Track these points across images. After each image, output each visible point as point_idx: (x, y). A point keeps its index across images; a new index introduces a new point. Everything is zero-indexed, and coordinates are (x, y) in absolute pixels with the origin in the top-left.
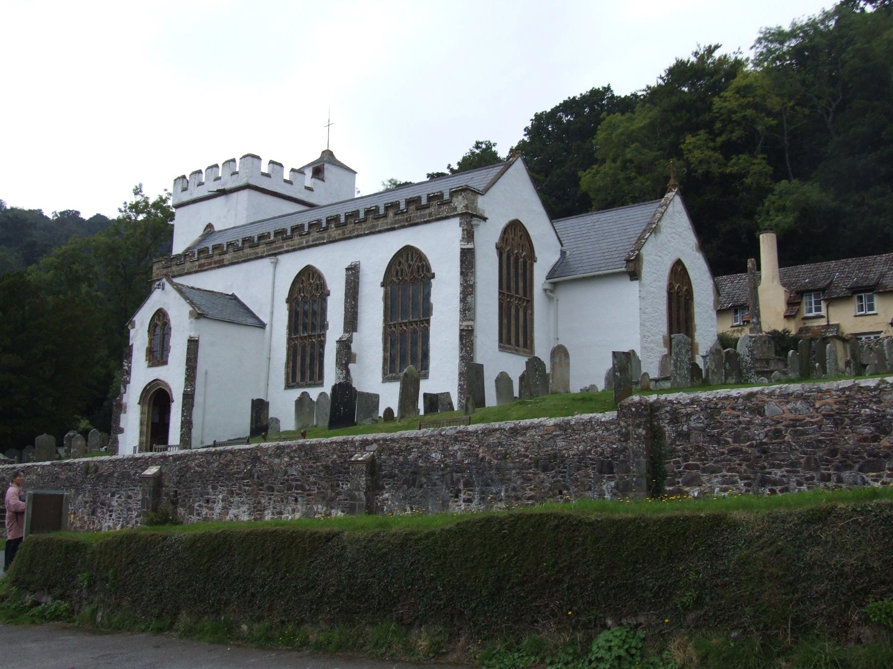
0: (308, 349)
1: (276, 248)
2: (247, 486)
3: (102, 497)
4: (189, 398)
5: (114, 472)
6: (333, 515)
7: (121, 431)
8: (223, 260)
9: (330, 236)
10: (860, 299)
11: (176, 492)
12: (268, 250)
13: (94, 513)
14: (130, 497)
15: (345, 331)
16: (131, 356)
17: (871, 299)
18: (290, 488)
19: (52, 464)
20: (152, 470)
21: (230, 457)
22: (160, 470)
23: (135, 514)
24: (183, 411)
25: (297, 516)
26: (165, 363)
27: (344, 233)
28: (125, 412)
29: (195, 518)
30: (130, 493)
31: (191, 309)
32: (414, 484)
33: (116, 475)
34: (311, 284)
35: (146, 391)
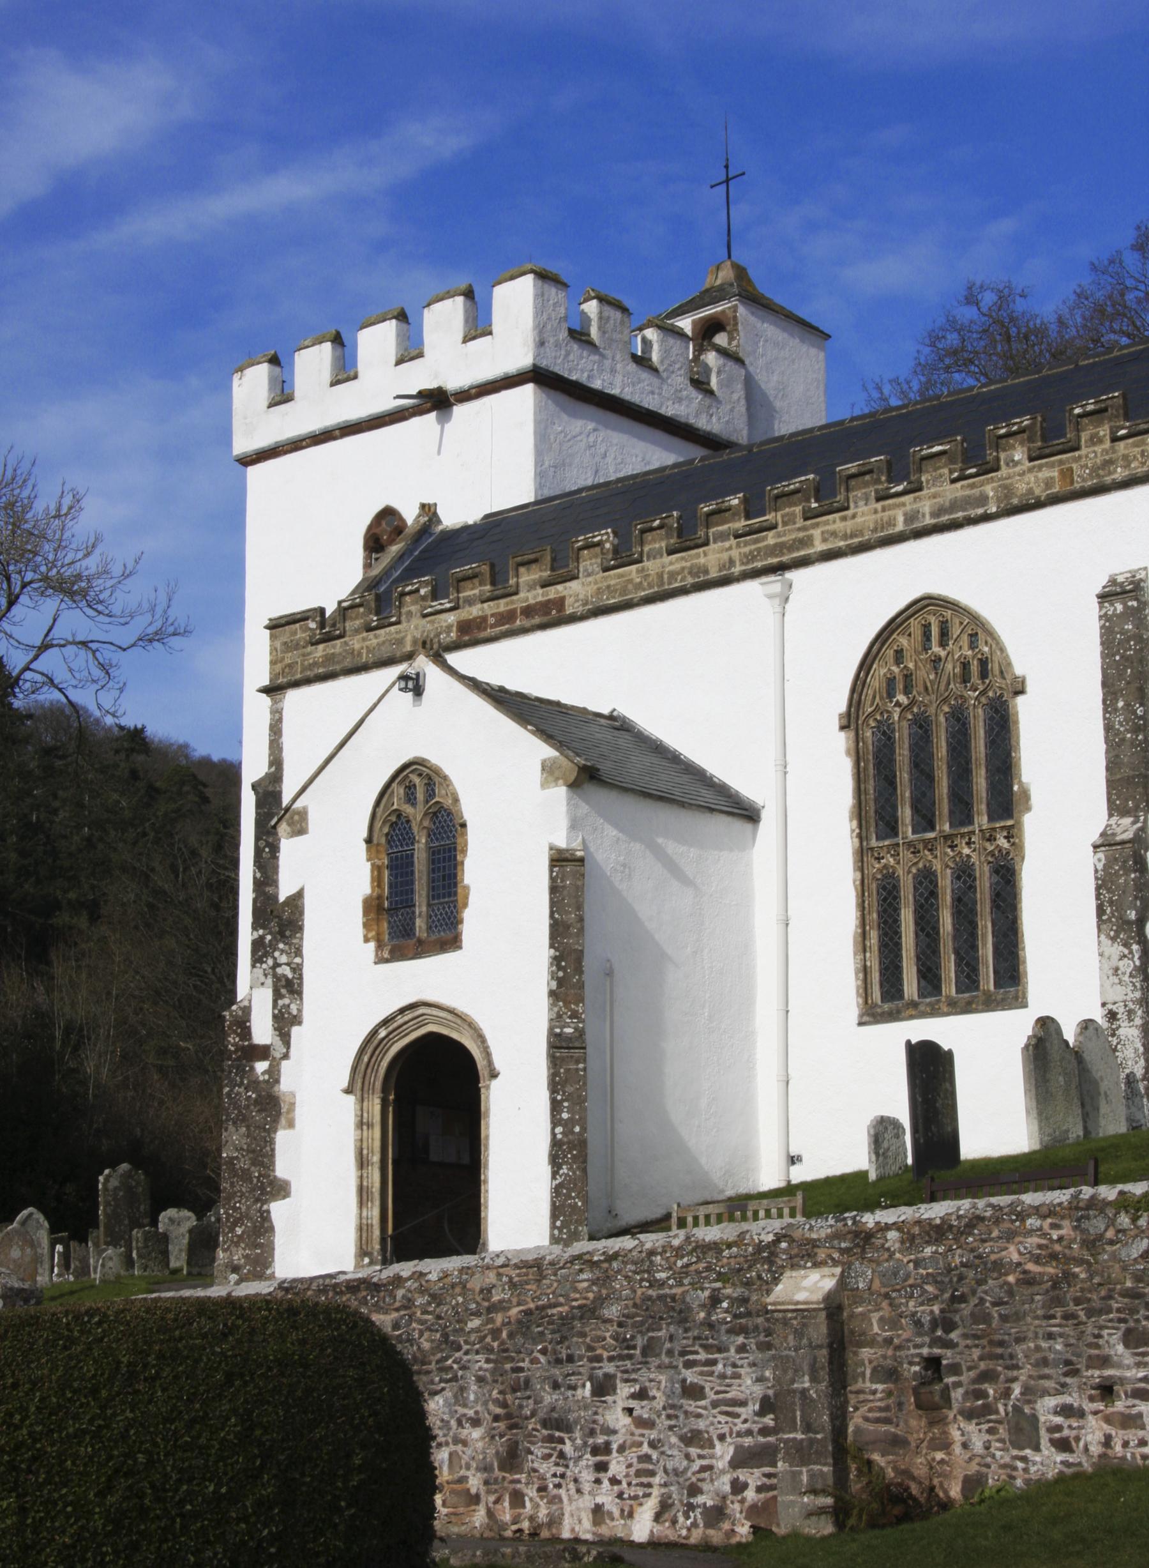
0: (946, 883)
1: (779, 548)
3: (549, 1398)
4: (569, 1056)
5: (600, 1301)
7: (281, 1190)
8: (560, 602)
9: (1007, 491)
11: (933, 1363)
12: (750, 558)
13: (512, 1459)
14: (693, 1392)
15: (1115, 808)
16: (300, 929)
19: (1074, 1204)
20: (808, 1286)
22: (842, 1282)
23: (723, 1453)
24: (555, 1106)
26: (451, 942)
27: (1067, 474)
28: (291, 1125)
30: (691, 1376)
31: (548, 752)
33: (613, 1311)
34: (936, 661)
35: (371, 1044)
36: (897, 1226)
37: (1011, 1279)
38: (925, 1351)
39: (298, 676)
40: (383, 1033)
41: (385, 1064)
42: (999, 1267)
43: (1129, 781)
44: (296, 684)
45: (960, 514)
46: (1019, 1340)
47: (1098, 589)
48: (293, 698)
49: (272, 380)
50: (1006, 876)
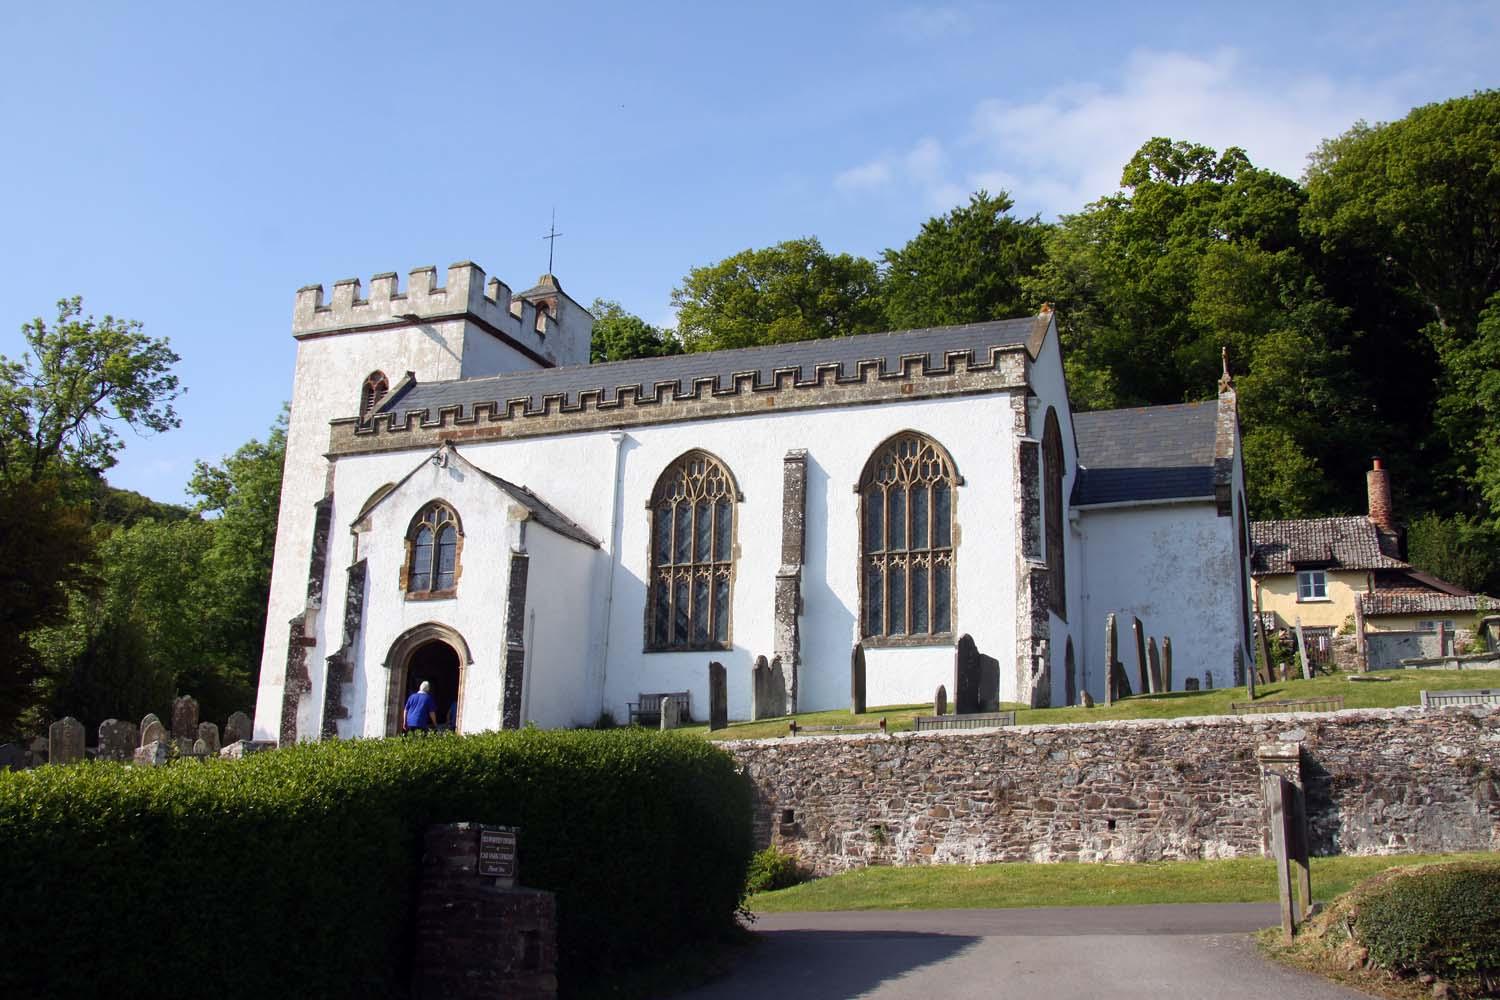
2: (982, 800)
6: (1208, 853)
8: (499, 430)
10: (1306, 580)
15: (786, 560)
17: (1320, 580)
18: (1095, 803)
21: (933, 749)
25: (1117, 853)
29: (844, 859)
32: (1400, 798)
35: (400, 643)
36: (775, 747)
37: (834, 774)
38: (786, 807)
39: (945, 391)
40: (407, 637)
41: (406, 653)
42: (828, 770)
43: (793, 547)
44: (345, 455)
45: (715, 412)
46: (835, 803)
47: (784, 456)
48: (341, 463)
49: (321, 300)
50: (942, 576)
